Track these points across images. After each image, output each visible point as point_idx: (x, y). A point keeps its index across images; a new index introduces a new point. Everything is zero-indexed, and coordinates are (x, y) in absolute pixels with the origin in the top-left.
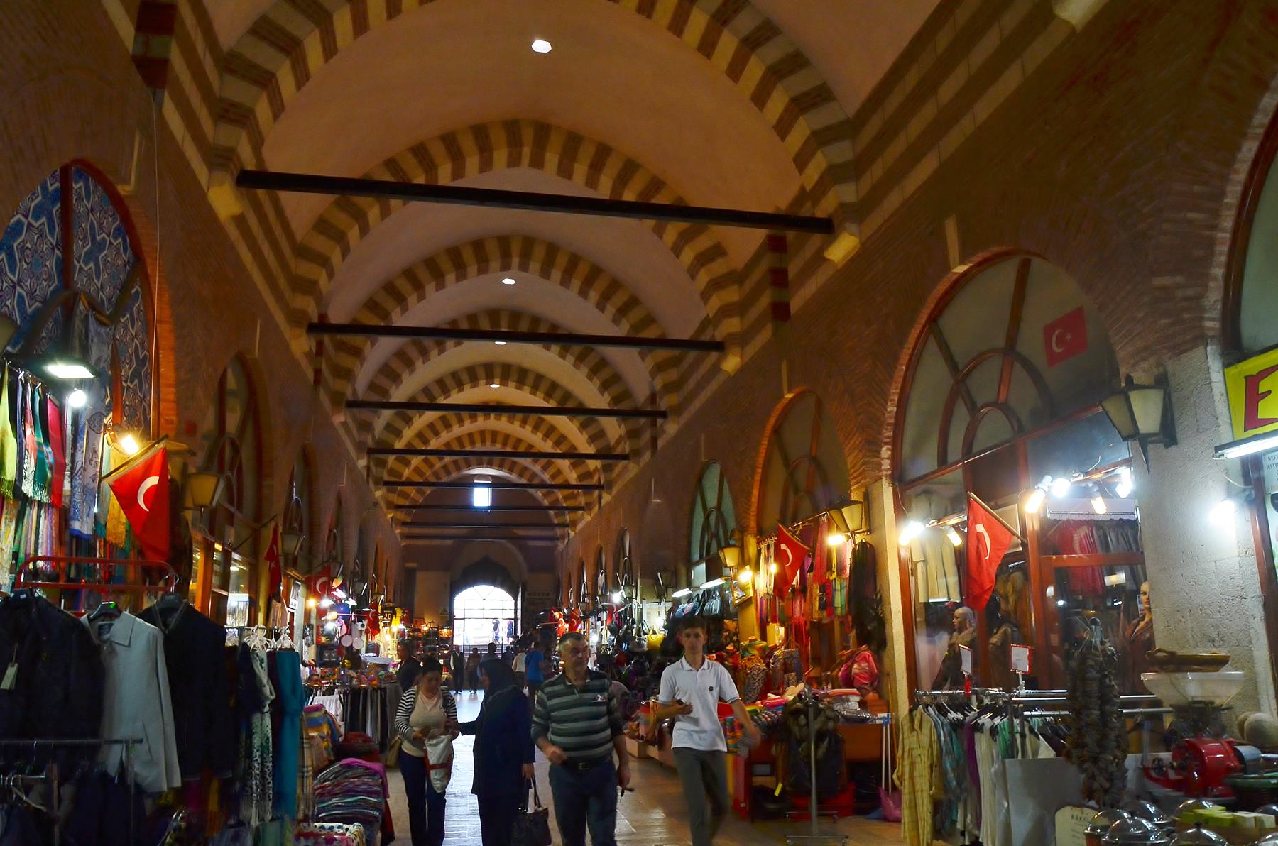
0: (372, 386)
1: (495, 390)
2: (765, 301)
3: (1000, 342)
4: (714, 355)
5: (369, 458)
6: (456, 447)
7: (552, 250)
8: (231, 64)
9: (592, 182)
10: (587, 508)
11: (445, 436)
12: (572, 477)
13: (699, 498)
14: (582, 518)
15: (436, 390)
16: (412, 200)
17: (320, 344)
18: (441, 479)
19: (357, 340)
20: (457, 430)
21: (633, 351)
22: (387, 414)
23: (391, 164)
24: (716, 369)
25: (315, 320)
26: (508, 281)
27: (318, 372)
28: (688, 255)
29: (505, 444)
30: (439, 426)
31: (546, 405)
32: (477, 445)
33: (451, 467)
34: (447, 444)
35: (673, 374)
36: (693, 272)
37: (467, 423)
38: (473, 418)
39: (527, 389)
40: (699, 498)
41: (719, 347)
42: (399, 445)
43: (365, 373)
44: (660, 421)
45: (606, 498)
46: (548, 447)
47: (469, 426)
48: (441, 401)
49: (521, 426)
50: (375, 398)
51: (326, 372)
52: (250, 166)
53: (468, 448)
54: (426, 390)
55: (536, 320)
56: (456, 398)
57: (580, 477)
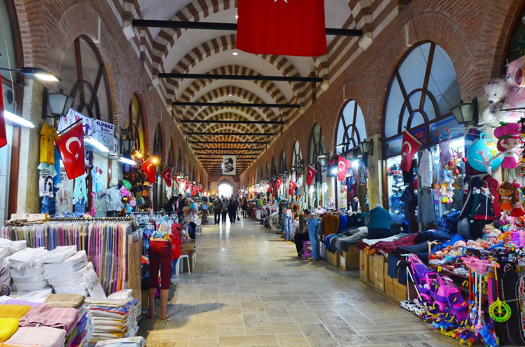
0: (183, 96)
1: (230, 97)
2: (310, 92)
3: (352, 123)
4: (356, 38)
5: (173, 107)
6: (214, 119)
10: (262, 149)
11: (211, 115)
12: (262, 131)
13: (312, 138)
14: (261, 153)
15: (207, 97)
20: (215, 113)
22: (188, 107)
24: (356, 46)
26: (235, 54)
31: (249, 103)
35: (301, 90)
39: (242, 96)
40: (312, 138)
41: (359, 33)
43: (178, 92)
44: (318, 84)
45: (268, 146)
46: (253, 119)
47: (220, 111)
48: (209, 102)
49: (243, 98)
50: (184, 101)
52: (161, 72)
53: (220, 120)
54: (203, 98)
55: (252, 71)
56: (215, 100)
57: (265, 131)
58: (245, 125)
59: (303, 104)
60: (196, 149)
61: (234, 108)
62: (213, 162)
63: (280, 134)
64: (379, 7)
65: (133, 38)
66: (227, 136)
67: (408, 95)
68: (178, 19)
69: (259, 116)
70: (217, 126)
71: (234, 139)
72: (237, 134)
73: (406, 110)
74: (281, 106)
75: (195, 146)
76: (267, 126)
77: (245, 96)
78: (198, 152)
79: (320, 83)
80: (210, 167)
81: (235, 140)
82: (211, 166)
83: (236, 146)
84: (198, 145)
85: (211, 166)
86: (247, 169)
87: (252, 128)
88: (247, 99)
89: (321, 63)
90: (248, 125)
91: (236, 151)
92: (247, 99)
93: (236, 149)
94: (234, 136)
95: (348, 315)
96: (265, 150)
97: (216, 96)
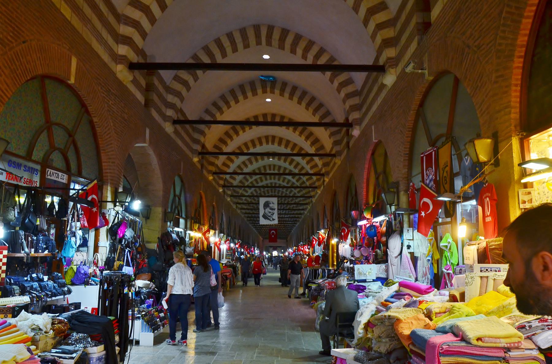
2: (345, 140)
7: (295, 89)
9: (304, 57)
16: (207, 70)
17: (202, 158)
19: (202, 127)
21: (322, 129)
23: (195, 57)
25: (176, 119)
28: (336, 84)
30: (247, 163)
32: (231, 166)
33: (259, 180)
34: (259, 169)
35: (338, 137)
36: (339, 90)
37: (260, 161)
38: (263, 159)
42: (230, 170)
54: (239, 148)
55: (283, 117)
58: (290, 177)
61: (276, 158)
63: (322, 188)
65: (132, 81)
66: (273, 189)
69: (303, 168)
70: (261, 178)
71: (280, 193)
72: (284, 187)
73: (44, 137)
74: (321, 156)
76: (312, 178)
77: (280, 144)
81: (282, 194)
83: (285, 201)
86: (297, 225)
87: (297, 181)
88: (283, 146)
89: (350, 106)
92: (283, 146)
93: (284, 204)
94: (281, 189)
97: (261, 144)
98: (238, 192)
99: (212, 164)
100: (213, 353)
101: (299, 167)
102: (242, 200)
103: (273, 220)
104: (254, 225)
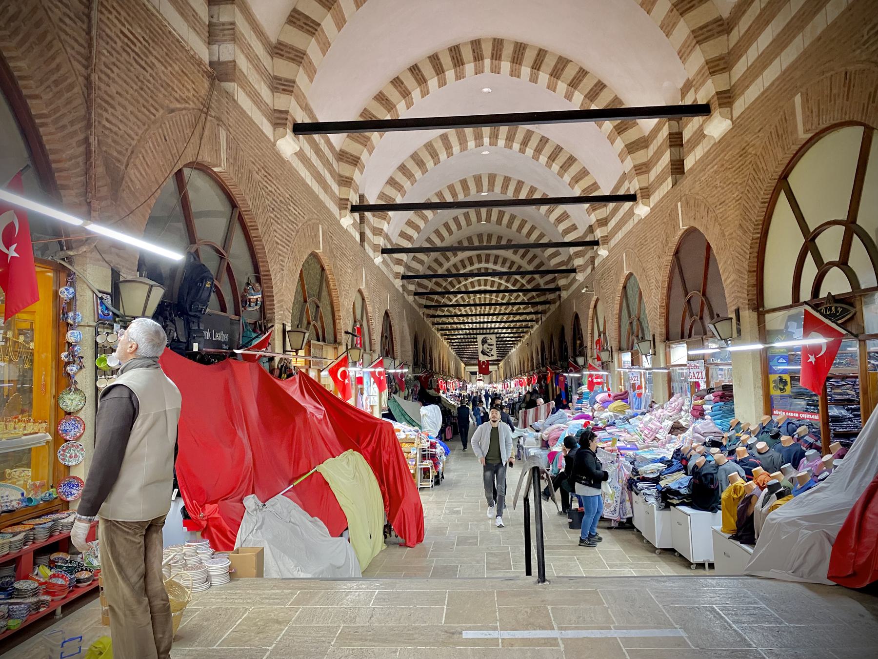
2: (666, 158)
4: (627, 205)
8: (278, 50)
17: (362, 219)
18: (437, 271)
24: (630, 213)
27: (362, 235)
29: (492, 286)
34: (448, 270)
40: (624, 301)
51: (368, 233)
59: (646, 193)
60: (427, 307)
62: (462, 329)
64: (744, 58)
67: (811, 231)
68: (428, 245)
75: (424, 302)
78: (431, 312)
79: (631, 203)
80: (457, 339)
82: (459, 337)
84: (432, 300)
85: (459, 337)
90: (515, 253)
91: (495, 317)
94: (489, 278)
95: (241, 153)
96: (540, 322)
98: (426, 287)
99: (378, 232)
100: (95, 591)
101: (587, 84)
102: (443, 311)
103: (492, 355)
104: (446, 335)
